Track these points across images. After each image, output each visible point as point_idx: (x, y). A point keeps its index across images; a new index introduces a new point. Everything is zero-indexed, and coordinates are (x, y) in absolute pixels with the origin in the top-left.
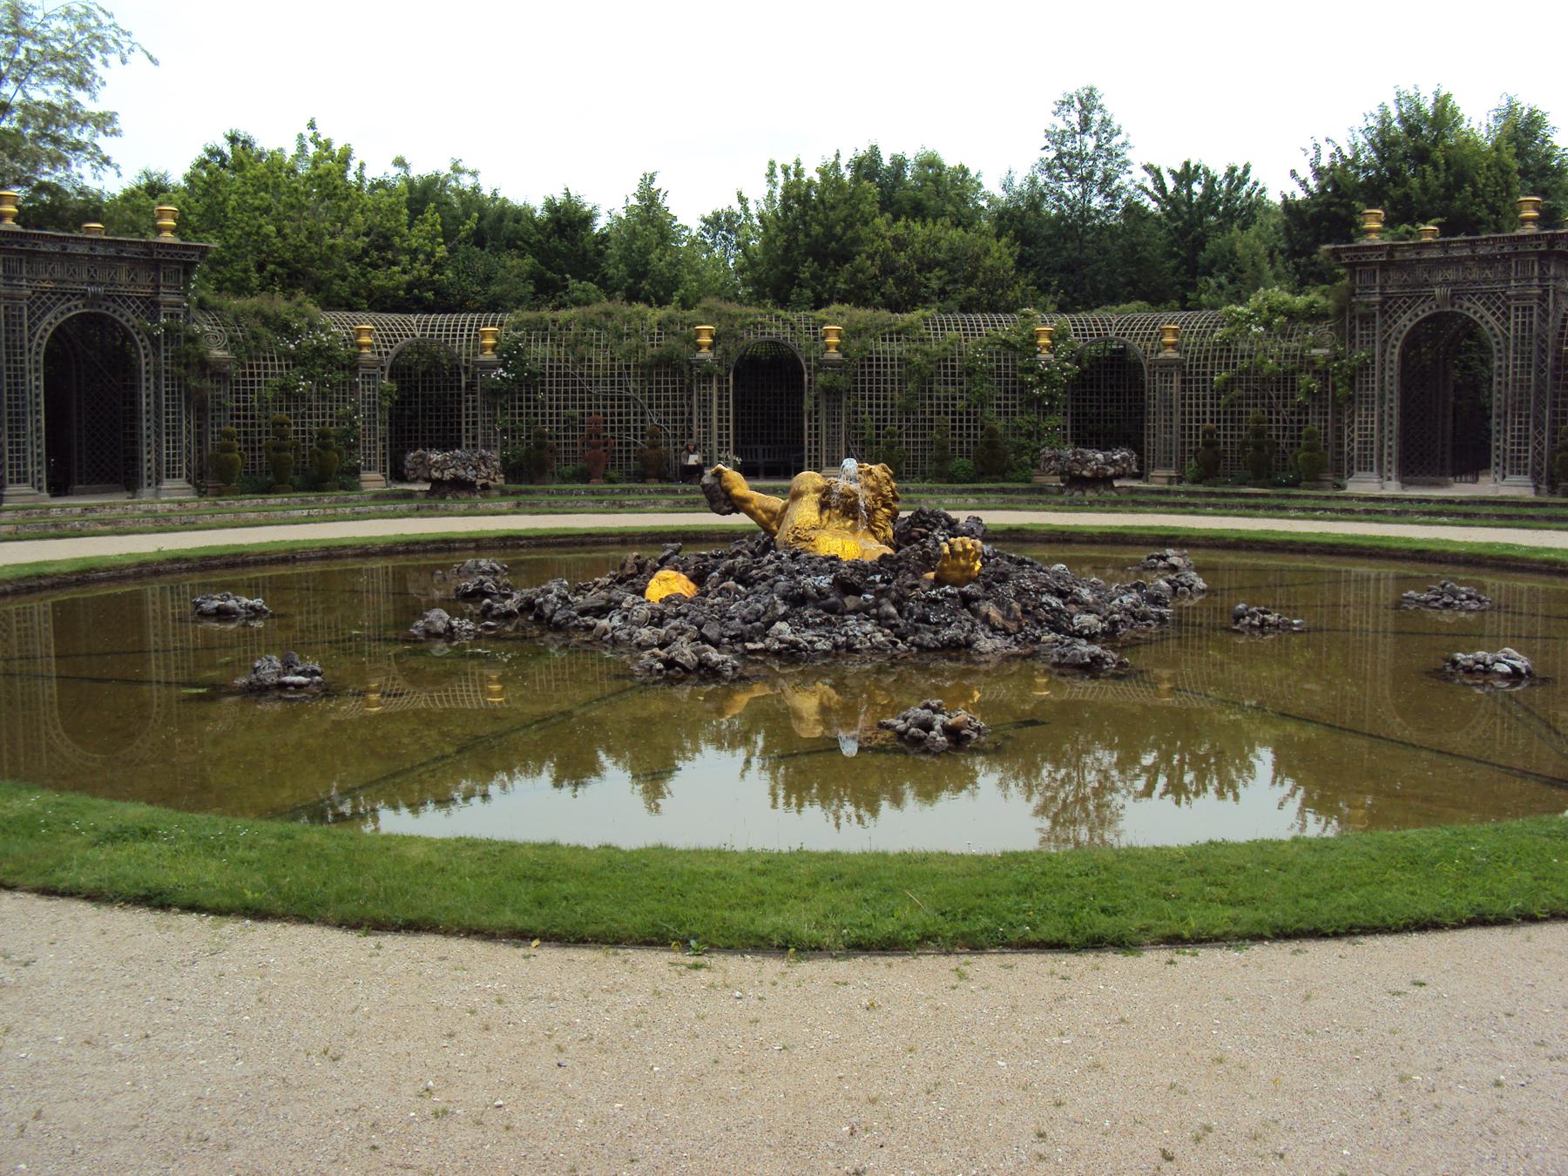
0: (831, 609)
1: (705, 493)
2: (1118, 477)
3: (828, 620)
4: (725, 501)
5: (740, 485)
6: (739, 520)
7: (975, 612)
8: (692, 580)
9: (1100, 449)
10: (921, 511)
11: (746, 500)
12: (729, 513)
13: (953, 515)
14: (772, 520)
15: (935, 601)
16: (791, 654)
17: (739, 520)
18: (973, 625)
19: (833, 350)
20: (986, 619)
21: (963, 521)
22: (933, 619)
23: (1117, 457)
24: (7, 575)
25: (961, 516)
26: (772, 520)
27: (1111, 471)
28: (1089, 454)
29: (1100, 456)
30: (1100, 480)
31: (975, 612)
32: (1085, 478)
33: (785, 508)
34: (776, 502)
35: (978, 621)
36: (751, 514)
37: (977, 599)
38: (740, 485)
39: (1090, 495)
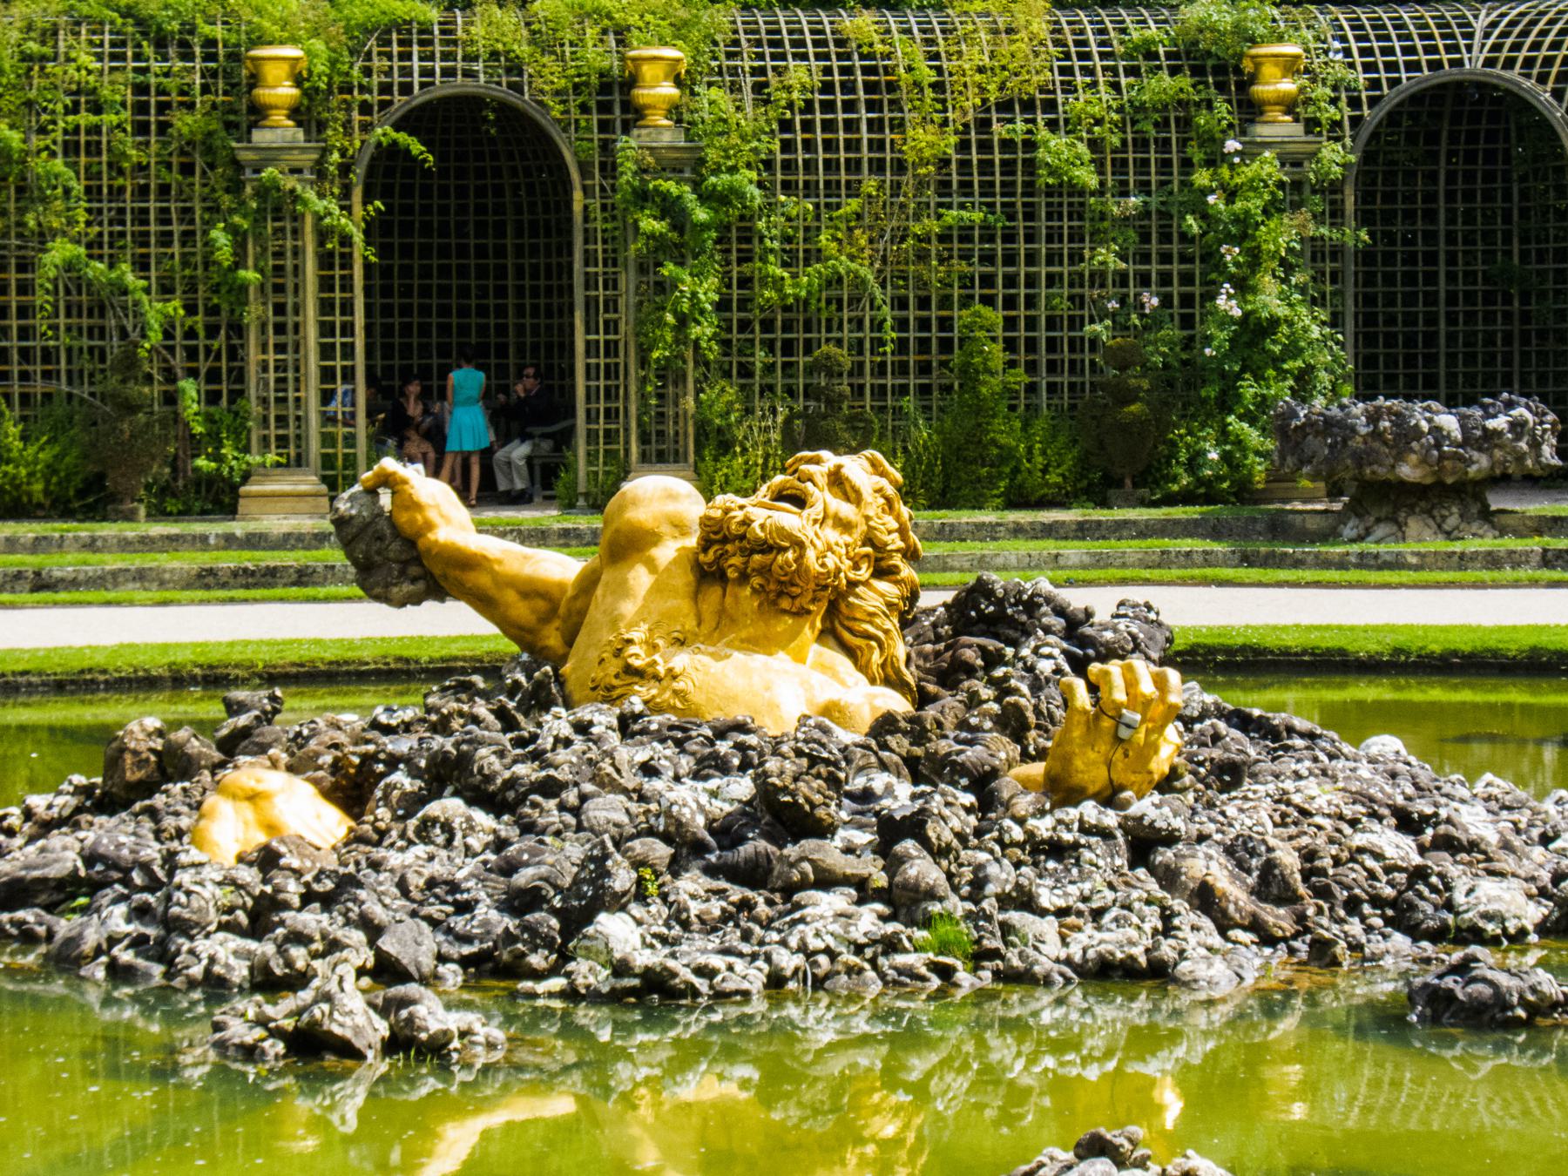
0: (753, 874)
1: (348, 545)
2: (1500, 480)
3: (745, 905)
4: (394, 561)
5: (446, 517)
6: (447, 625)
7: (1169, 878)
8: (330, 794)
9: (1450, 403)
10: (982, 589)
11: (467, 562)
12: (416, 600)
13: (1076, 599)
14: (546, 619)
15: (1057, 849)
16: (653, 994)
17: (447, 625)
18: (1167, 916)
19: (279, 117)
20: (1205, 899)
21: (1102, 615)
22: (1046, 899)
23: (1500, 423)
24: (9, 667)
25: (1100, 602)
26: (546, 619)
27: (1480, 463)
28: (1420, 415)
29: (1449, 422)
30: (1455, 495)
31: (1169, 878)
32: (1403, 486)
33: (588, 583)
34: (560, 567)
35: (1179, 904)
36: (484, 603)
37: (1171, 839)
38: (446, 517)
39: (1421, 540)
